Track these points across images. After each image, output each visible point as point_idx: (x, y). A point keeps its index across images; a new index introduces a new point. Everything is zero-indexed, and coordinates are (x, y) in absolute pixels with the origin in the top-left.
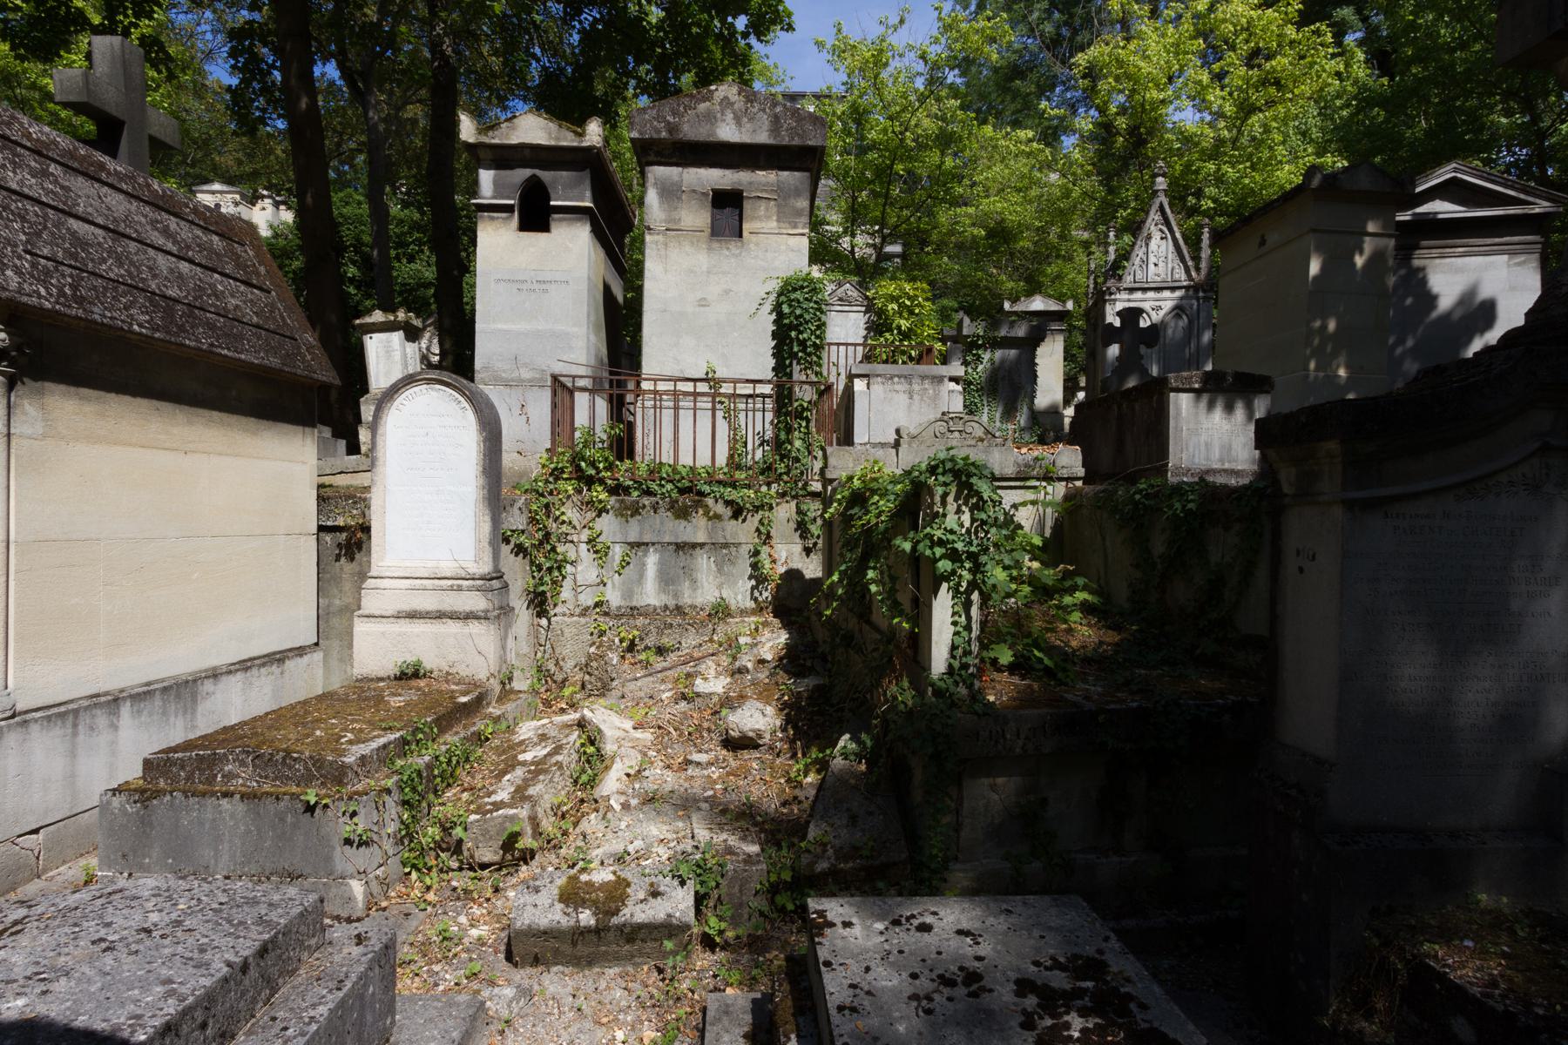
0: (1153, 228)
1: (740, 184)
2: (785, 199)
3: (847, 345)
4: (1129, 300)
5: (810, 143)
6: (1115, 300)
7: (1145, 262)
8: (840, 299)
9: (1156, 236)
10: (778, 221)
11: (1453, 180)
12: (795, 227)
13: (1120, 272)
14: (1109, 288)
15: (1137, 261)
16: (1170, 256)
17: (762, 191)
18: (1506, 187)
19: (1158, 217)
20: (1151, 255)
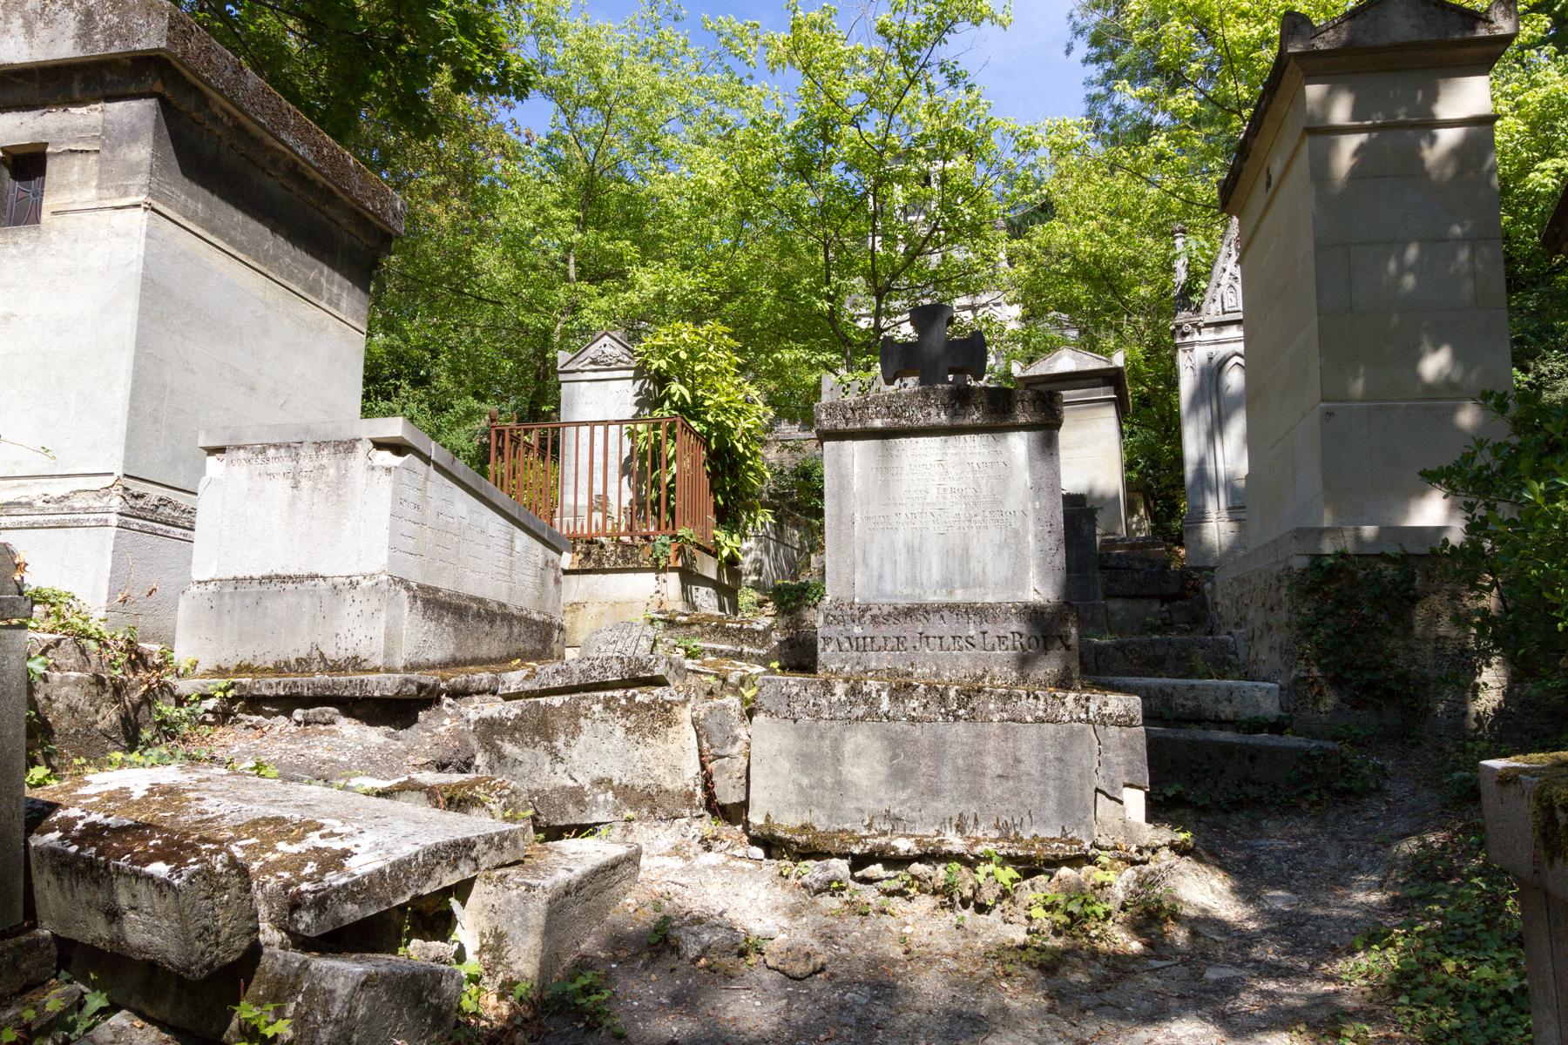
1: (44, 135)
2: (112, 149)
3: (606, 423)
4: (1217, 342)
5: (138, 47)
6: (1192, 344)
8: (594, 362)
10: (99, 187)
12: (126, 194)
13: (1195, 299)
14: (1179, 327)
17: (77, 141)
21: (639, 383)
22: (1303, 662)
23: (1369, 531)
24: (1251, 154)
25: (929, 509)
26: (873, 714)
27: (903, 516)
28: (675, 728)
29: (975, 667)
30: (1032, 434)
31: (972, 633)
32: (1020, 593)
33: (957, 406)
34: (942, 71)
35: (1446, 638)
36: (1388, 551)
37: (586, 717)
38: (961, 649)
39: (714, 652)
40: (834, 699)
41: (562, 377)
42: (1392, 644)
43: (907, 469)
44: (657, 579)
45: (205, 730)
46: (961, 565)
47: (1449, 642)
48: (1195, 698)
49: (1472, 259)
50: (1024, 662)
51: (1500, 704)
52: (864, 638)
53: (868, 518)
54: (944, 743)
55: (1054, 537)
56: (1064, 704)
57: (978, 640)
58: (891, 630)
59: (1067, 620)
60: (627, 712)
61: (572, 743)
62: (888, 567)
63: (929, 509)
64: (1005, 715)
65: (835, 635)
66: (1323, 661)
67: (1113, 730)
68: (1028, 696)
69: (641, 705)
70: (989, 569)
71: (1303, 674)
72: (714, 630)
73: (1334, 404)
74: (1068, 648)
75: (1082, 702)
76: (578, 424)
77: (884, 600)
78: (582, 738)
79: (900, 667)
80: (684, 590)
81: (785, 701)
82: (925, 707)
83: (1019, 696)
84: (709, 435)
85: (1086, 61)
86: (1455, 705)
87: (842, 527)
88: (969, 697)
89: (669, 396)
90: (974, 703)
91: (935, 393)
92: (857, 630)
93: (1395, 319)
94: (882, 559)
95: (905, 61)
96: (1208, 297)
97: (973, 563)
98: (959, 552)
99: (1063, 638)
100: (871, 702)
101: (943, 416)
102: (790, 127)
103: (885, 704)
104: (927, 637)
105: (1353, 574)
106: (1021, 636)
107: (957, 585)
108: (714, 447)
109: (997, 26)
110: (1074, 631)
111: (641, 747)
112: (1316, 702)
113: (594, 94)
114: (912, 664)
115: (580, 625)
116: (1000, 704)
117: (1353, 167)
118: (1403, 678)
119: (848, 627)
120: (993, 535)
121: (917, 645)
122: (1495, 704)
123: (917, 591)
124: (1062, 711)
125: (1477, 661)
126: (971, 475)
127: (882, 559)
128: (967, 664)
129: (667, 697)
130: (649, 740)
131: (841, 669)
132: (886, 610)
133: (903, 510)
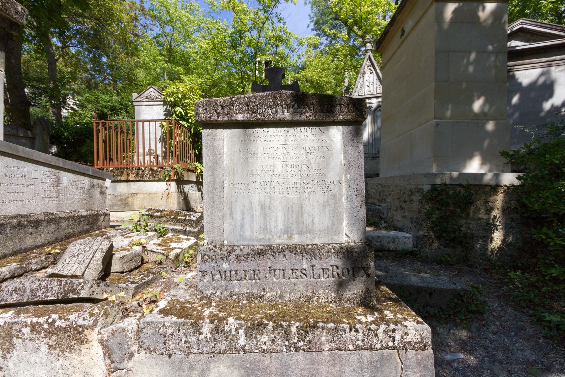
0: (366, 68)
7: (363, 85)
8: (147, 98)
9: (368, 72)
11: (521, 30)
13: (351, 91)
15: (359, 85)
16: (375, 82)
18: (552, 29)
19: (368, 63)
20: (365, 82)
21: (165, 107)
22: (426, 229)
23: (455, 174)
24: (395, 24)
25: (275, 179)
26: (232, 348)
27: (258, 183)
28: (86, 346)
29: (307, 290)
30: (346, 128)
31: (305, 266)
32: (336, 237)
33: (296, 106)
34: (276, 16)
35: (481, 219)
36: (463, 183)
37: (18, 337)
38: (297, 278)
39: (173, 230)
40: (202, 337)
41: (135, 103)
42: (462, 221)
43: (261, 150)
44: (167, 184)
45: (91, 202)
46: (297, 218)
47: (482, 220)
48: (380, 242)
49: (495, 61)
50: (340, 285)
51: (500, 245)
52: (230, 271)
53: (234, 185)
54: (288, 369)
55: (359, 198)
56: (376, 335)
57: (309, 271)
58: (250, 265)
59: (368, 257)
60: (49, 334)
61: (8, 356)
62: (247, 220)
63: (275, 179)
64: (333, 345)
65: (209, 270)
66: (435, 229)
67: (411, 353)
68: (351, 330)
69: (59, 329)
70: (316, 220)
71: (426, 234)
72: (173, 220)
73: (440, 120)
74: (368, 276)
75: (390, 333)
76: (144, 121)
77: (245, 243)
78: (15, 352)
79: (256, 292)
80: (179, 187)
81: (162, 340)
82: (273, 341)
83: (344, 330)
84: (191, 128)
85: (312, 30)
86: (483, 245)
87: (215, 191)
88: (307, 332)
89: (175, 112)
90: (310, 336)
91: (280, 96)
92: (225, 266)
93: (464, 85)
94: (243, 214)
95: (265, 12)
96: (354, 90)
97: (306, 217)
98: (296, 209)
99: (365, 269)
100: (231, 338)
101: (286, 114)
102: (230, 32)
103: (242, 340)
104: (274, 270)
105: (447, 193)
106: (337, 268)
107: (295, 232)
108: (192, 132)
109: (293, 3)
110: (372, 264)
111: (61, 359)
112: (431, 245)
113: (168, 19)
114: (264, 290)
115: (135, 202)
116: (329, 337)
117: (452, 18)
118: (465, 235)
119: (219, 263)
120: (319, 197)
121: (268, 275)
122: (498, 245)
123: (268, 236)
124: (375, 341)
125: (493, 228)
126: (304, 155)
127: (243, 214)
128: (301, 288)
129: (81, 322)
130: (67, 354)
131: (214, 294)
132: (246, 250)
133: (258, 179)
